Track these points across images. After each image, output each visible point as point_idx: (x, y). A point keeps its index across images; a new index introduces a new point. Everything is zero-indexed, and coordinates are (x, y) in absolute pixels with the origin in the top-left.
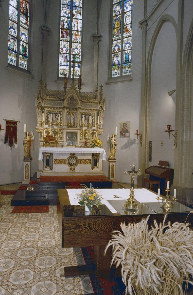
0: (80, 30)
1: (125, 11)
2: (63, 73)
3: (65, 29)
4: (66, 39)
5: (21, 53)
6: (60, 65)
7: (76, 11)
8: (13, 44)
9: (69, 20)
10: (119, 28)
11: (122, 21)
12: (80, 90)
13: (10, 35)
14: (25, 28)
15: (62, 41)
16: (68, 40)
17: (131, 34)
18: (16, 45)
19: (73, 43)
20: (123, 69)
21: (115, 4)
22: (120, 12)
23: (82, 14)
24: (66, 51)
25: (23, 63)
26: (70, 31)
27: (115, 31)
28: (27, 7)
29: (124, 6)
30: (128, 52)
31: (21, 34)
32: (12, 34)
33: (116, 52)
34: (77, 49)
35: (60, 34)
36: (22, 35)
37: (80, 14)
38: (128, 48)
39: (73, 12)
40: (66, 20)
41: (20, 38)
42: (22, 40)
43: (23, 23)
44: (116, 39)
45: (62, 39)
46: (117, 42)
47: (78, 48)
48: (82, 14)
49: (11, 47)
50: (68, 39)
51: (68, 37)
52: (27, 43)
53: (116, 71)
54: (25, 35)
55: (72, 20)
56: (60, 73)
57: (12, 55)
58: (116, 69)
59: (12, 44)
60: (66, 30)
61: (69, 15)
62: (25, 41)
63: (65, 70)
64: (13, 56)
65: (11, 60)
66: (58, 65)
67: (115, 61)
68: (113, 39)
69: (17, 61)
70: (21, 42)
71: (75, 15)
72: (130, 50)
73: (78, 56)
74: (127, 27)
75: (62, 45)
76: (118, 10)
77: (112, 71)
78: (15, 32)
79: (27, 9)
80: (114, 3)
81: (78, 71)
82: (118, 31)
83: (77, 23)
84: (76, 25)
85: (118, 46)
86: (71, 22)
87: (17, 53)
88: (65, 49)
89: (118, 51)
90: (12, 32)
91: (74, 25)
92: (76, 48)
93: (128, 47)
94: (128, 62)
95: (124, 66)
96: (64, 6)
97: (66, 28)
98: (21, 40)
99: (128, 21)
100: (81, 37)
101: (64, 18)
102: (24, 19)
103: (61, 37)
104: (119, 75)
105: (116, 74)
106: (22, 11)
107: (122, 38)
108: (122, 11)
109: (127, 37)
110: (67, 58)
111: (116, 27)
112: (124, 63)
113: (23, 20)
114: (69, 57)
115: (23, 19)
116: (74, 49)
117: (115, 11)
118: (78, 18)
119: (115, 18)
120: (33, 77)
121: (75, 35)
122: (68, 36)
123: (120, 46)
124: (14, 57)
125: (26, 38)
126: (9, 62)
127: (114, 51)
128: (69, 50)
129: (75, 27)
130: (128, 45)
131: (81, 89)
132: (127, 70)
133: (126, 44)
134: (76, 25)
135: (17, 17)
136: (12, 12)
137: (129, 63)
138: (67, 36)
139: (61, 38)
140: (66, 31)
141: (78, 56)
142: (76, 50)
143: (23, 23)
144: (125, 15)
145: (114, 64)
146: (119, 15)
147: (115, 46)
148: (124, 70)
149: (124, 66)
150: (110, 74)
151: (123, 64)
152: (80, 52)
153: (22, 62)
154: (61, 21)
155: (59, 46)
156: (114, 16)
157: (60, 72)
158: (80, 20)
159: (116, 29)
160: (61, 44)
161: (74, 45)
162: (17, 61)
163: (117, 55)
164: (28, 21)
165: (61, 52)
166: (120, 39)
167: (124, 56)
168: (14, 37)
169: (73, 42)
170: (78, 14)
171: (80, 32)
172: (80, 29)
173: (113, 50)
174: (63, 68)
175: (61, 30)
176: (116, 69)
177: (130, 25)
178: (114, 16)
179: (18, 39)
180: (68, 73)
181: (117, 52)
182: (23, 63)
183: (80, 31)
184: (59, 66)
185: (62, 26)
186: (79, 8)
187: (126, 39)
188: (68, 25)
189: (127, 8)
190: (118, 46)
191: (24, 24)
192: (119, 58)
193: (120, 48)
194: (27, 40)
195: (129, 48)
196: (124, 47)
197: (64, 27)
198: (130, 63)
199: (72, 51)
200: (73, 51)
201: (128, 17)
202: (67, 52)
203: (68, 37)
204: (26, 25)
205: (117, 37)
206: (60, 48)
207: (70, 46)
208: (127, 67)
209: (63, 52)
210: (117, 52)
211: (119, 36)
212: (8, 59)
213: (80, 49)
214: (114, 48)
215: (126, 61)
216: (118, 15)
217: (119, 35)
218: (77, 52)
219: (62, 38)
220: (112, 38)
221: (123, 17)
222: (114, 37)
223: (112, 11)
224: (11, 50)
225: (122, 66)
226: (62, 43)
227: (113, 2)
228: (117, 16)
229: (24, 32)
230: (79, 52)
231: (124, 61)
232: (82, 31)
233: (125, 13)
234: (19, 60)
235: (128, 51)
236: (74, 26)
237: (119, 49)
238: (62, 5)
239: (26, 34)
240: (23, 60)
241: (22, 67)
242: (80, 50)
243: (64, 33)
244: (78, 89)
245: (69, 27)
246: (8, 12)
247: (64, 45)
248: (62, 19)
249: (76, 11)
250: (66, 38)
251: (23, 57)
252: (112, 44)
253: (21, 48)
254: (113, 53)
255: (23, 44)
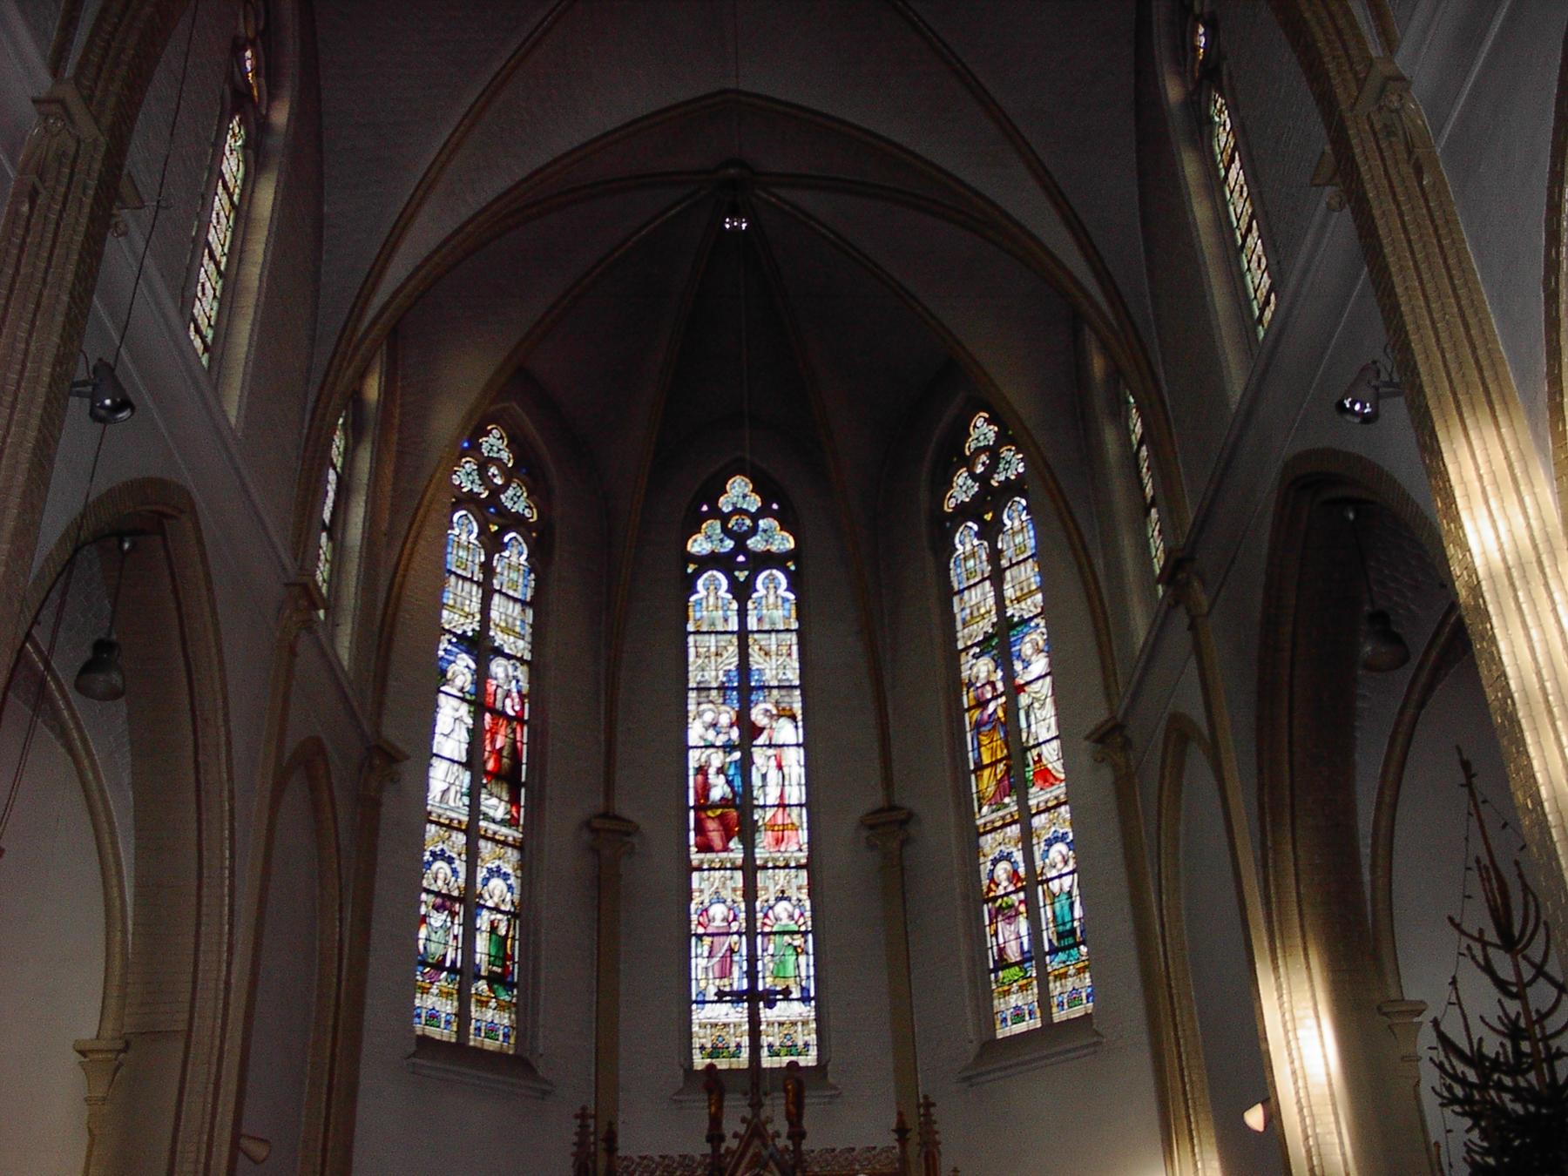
0: (794, 801)
1: (1020, 681)
2: (714, 1047)
3: (714, 806)
4: (724, 855)
5: (483, 973)
6: (697, 1002)
7: (770, 706)
8: (441, 932)
9: (737, 755)
10: (1001, 766)
11: (1010, 725)
12: (797, 1145)
13: (428, 892)
14: (504, 843)
15: (700, 869)
16: (732, 861)
17: (1063, 789)
18: (456, 937)
19: (760, 875)
20: (1051, 985)
21: (967, 648)
22: (994, 688)
23: (799, 718)
24: (725, 919)
25: (983, 431)
26: (739, 817)
27: (987, 782)
28: (514, 741)
29: (1011, 654)
30: (1066, 889)
31: (481, 874)
32: (440, 883)
33: (1001, 891)
34: (789, 899)
35: (692, 834)
36: (486, 881)
37: (793, 718)
38: (1060, 865)
39: (753, 717)
40: (717, 759)
41: (481, 896)
42: (490, 904)
43: (494, 821)
44: (993, 822)
45: (702, 862)
46: (999, 836)
47: (792, 893)
48: (799, 718)
49: (432, 947)
50: (731, 855)
51: (734, 844)
52: (512, 915)
53: (1014, 1000)
54: (506, 876)
55: (751, 754)
56: (702, 1048)
57: (434, 990)
58: (1015, 987)
59: (437, 933)
60: (719, 812)
61: (735, 734)
62: (503, 908)
63: (726, 1025)
64: (441, 993)
65: (433, 1017)
66: (685, 1003)
67: (1001, 941)
68: (980, 822)
69: (463, 1016)
70: (485, 913)
71: (762, 730)
72: (1072, 873)
73: (798, 941)
74: (1039, 755)
75: (701, 891)
76: (983, 675)
77: (996, 1002)
78: (454, 872)
79: (515, 753)
80: (960, 646)
81: (805, 1023)
82: (1000, 782)
83: (780, 767)
84: (773, 776)
85: (1007, 857)
86: (746, 765)
87: (465, 973)
88: (718, 911)
89: (1011, 888)
90: (441, 876)
91: (764, 776)
92: (782, 897)
93: (1059, 859)
94: (1071, 941)
95: (1054, 964)
96: (704, 694)
97: (722, 798)
98: (484, 907)
99: (1042, 724)
100: (803, 836)
101: (709, 751)
102: (500, 799)
103: (693, 849)
104: (1037, 1023)
105: (1018, 1016)
106: (490, 765)
107: (1025, 817)
108: (1003, 679)
109: (1048, 810)
110: (736, 958)
111: (986, 760)
112: (1054, 951)
113: (495, 806)
114: (744, 952)
115: (494, 801)
116: (772, 902)
117: (970, 684)
118: (778, 740)
119: (976, 714)
120: (545, 1093)
121: (772, 827)
122: (736, 839)
123: (1018, 856)
124: (449, 995)
125: (510, 887)
126: (419, 1029)
127: (990, 890)
128: (742, 915)
129: (768, 789)
130: (1060, 847)
131: (803, 1135)
132: (1073, 994)
133: (1049, 843)
134: (773, 776)
135: (466, 800)
136: (445, 786)
137: (1077, 945)
138: (729, 839)
139: (696, 857)
140: (721, 818)
141: (798, 941)
142: (782, 909)
143: (494, 821)
144: (1024, 700)
145: (1002, 963)
146: (994, 698)
147: (995, 862)
148: (1055, 988)
149: (1054, 964)
150: (988, 1017)
151: (1049, 953)
152: (808, 914)
153: (489, 1014)
154: (691, 772)
155: (689, 899)
156: (969, 709)
157: (696, 1043)
158: (793, 750)
159: (986, 773)
160: (695, 885)
161: (770, 884)
162: (463, 1016)
163: (1011, 906)
164: (518, 808)
165: (701, 930)
166: (1014, 822)
167: (1046, 914)
168: (448, 897)
169: (764, 868)
170: (782, 720)
171: (795, 811)
172: (796, 794)
173: (985, 882)
174: (713, 1020)
175: (692, 814)
176: (1015, 987)
177: (1055, 744)
178: (969, 709)
179: (468, 902)
180: (745, 1041)
181: (1007, 894)
182: (493, 1019)
183: (800, 805)
184: (690, 1011)
185: (696, 792)
186: (783, 692)
187: (1043, 816)
188: (729, 783)
189: (1027, 664)
190: (1007, 857)
191: (503, 822)
192: (1023, 925)
193: (1022, 871)
194: (516, 898)
195: (1066, 863)
196: (1039, 863)
197: (707, 797)
198: (1083, 949)
199: (760, 915)
200: (766, 916)
201: (1036, 705)
202: (735, 927)
203: (734, 844)
204: (510, 826)
205: (1001, 813)
206: (693, 907)
207: (750, 893)
208: (1072, 971)
209: (710, 930)
210: (1007, 894)
211: (1006, 806)
212: (411, 1012)
213: (804, 895)
214: (992, 871)
215: (1060, 936)
216: (989, 701)
217: (1007, 800)
218: (791, 917)
219: (701, 856)
220: (971, 816)
221: (1012, 708)
222: (985, 810)
223: (956, 684)
224: (431, 966)
225: (1041, 968)
226: (702, 879)
227: (956, 640)
228: (982, 704)
229: (497, 862)
230: (802, 915)
231: (1050, 941)
232: (809, 805)
233: (1021, 689)
234: (473, 1008)
235: (1067, 881)
236: (764, 786)
237: (1015, 872)
238: (692, 695)
239: (507, 868)
240: (493, 1003)
241: (489, 1044)
242: (807, 904)
243: (711, 825)
244: (789, 1137)
245: (735, 793)
246: (426, 788)
247: (713, 892)
248: (694, 758)
249: (770, 706)
250: (726, 849)
251: (491, 989)
252: (977, 850)
253: (482, 944)
254: (987, 901)
255: (492, 922)
